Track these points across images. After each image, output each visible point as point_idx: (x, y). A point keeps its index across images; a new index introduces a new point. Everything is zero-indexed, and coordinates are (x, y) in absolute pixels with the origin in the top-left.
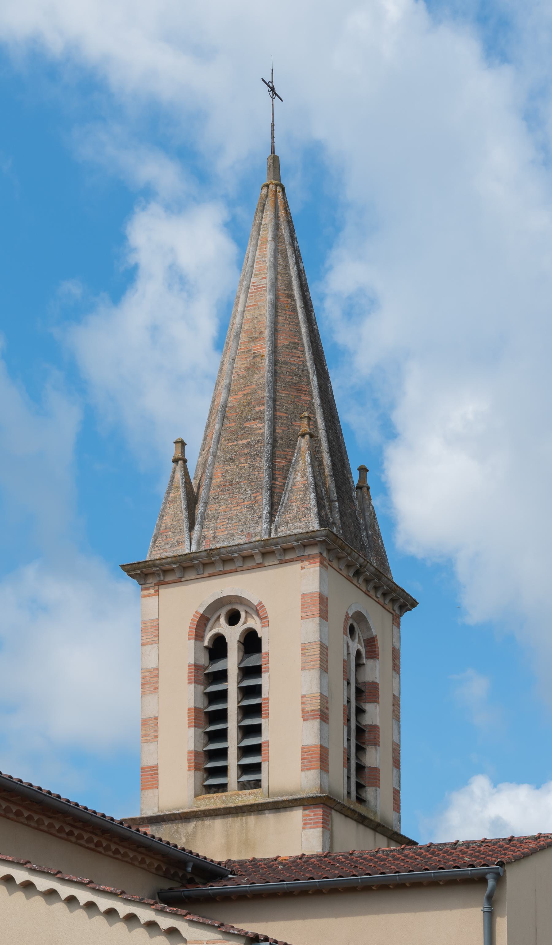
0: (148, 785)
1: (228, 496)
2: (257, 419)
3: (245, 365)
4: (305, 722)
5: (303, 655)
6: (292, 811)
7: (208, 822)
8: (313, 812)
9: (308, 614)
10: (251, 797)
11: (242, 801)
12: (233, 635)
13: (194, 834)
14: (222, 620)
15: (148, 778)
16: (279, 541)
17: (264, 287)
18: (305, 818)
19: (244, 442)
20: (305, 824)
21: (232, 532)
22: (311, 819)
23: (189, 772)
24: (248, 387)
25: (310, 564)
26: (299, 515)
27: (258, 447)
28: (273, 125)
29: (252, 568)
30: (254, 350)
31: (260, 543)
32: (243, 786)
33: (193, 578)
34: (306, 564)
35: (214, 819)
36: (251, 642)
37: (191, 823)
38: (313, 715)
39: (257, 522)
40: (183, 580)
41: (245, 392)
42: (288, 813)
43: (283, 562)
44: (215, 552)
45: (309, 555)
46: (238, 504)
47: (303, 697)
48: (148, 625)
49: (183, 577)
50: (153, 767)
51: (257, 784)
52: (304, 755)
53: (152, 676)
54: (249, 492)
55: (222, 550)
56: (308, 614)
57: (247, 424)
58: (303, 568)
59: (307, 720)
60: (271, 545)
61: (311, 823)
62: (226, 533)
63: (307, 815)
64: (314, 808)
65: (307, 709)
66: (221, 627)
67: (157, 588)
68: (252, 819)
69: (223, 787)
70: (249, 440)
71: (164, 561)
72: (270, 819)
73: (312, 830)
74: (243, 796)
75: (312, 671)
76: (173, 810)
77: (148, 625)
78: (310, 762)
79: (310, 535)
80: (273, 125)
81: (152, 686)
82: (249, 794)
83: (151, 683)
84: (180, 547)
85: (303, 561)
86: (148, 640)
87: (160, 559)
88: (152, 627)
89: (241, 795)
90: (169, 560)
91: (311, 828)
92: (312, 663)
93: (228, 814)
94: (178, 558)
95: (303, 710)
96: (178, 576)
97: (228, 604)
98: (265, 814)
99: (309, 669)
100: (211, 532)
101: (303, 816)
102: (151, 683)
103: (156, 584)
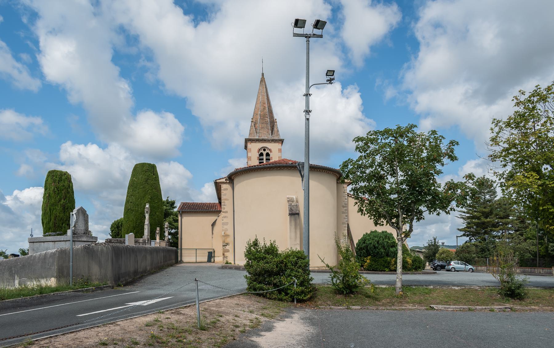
12: (265, 153)
36: (268, 155)
66: (262, 151)
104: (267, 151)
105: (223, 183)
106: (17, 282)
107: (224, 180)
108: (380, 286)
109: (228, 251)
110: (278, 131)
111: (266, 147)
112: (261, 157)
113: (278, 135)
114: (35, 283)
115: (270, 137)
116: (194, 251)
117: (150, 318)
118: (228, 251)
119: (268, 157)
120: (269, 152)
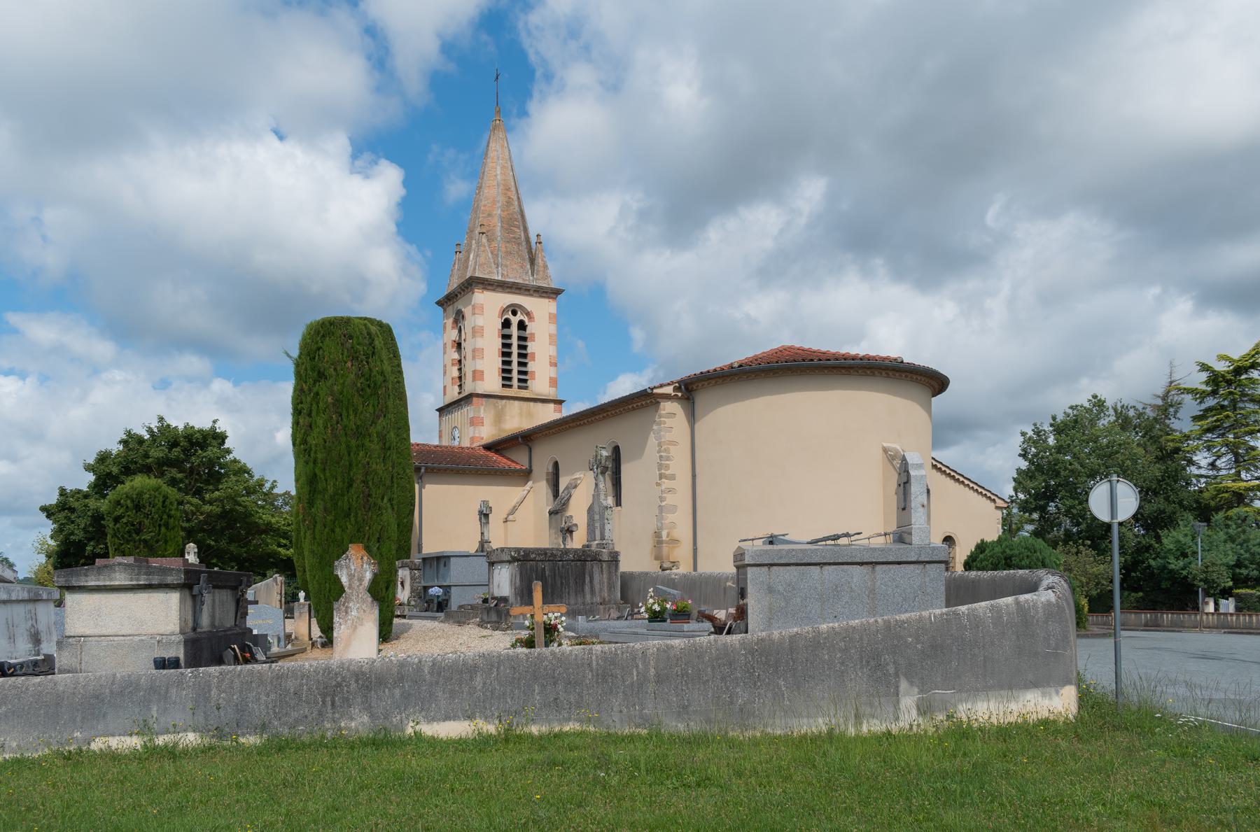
12: (515, 321)
32: (519, 387)
36: (522, 326)
51: (526, 388)
66: (510, 316)
68: (532, 404)
69: (510, 386)
72: (540, 405)
104: (520, 316)
105: (667, 397)
106: (908, 702)
107: (669, 390)
109: (673, 509)
110: (545, 267)
111: (520, 306)
112: (506, 331)
113: (546, 277)
114: (821, 721)
116: (484, 580)
118: (673, 509)
119: (522, 333)
120: (526, 319)
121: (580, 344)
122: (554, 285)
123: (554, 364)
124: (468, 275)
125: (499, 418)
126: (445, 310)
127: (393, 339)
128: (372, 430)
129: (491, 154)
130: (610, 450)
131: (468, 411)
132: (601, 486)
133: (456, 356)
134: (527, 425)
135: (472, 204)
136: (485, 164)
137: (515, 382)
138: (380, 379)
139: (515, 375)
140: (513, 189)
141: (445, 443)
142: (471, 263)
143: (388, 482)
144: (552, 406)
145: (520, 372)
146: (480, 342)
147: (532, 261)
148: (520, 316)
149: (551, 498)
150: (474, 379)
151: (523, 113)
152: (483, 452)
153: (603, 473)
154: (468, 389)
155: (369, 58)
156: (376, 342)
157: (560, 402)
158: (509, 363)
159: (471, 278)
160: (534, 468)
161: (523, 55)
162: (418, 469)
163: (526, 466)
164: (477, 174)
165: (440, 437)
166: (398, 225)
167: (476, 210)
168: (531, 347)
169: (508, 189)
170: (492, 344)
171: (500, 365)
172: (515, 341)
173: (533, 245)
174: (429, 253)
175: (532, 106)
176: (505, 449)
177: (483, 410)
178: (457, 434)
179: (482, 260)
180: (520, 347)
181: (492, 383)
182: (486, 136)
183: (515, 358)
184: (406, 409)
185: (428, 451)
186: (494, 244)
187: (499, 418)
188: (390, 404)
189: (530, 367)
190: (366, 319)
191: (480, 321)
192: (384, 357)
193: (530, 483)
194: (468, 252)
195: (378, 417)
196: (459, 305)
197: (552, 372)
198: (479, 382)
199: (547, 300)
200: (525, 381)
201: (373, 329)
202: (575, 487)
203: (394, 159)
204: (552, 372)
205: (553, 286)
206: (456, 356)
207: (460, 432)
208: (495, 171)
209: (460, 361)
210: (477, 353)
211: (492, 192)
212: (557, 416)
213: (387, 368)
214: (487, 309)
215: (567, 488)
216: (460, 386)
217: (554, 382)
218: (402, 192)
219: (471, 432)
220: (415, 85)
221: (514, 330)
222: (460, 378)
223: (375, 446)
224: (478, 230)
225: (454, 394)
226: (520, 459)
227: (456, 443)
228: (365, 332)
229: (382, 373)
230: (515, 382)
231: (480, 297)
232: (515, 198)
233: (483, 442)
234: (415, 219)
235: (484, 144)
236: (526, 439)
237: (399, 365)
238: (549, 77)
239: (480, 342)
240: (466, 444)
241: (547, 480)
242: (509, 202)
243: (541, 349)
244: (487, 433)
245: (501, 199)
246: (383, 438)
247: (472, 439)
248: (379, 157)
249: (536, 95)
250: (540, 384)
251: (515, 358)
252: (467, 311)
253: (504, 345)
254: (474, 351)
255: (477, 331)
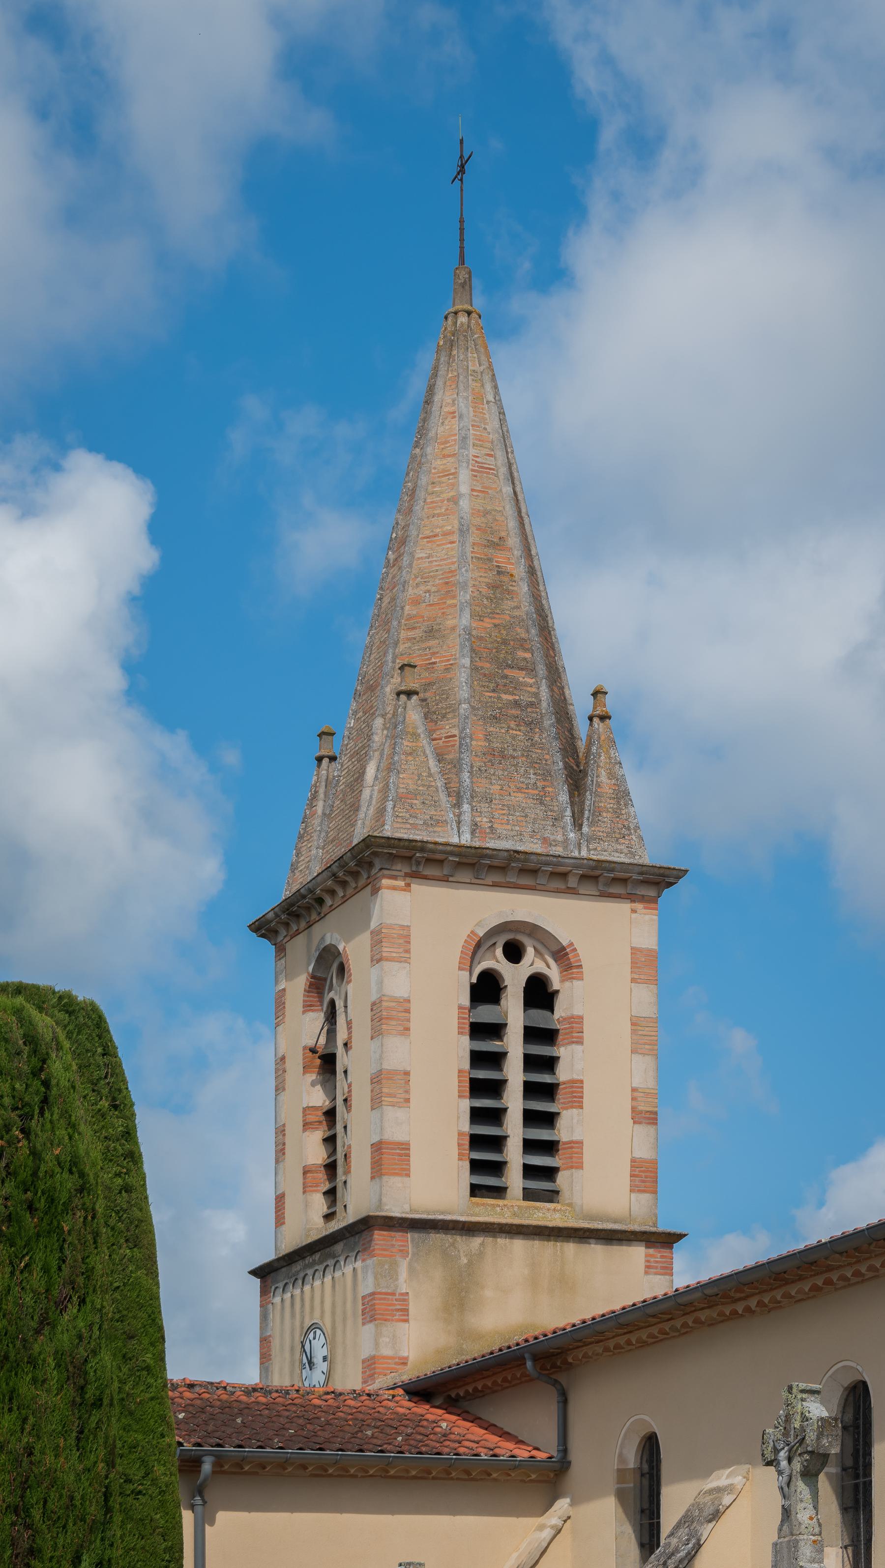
0: (395, 1169)
1: (501, 773)
2: (522, 669)
3: (486, 580)
4: (636, 1126)
5: (634, 1032)
6: (630, 1246)
7: (502, 1241)
8: (660, 1252)
9: (642, 977)
10: (558, 1215)
11: (543, 1218)
12: (514, 978)
13: (481, 1254)
14: (499, 952)
15: (395, 1159)
16: (618, 867)
17: (493, 469)
18: (649, 1258)
19: (511, 698)
20: (647, 1267)
21: (517, 828)
22: (657, 1262)
23: (460, 1163)
24: (497, 616)
25: (645, 908)
26: (614, 832)
27: (533, 712)
28: (462, 221)
29: (557, 892)
30: (496, 562)
31: (591, 862)
32: (529, 1195)
33: (469, 881)
34: (639, 906)
35: (511, 1238)
36: (539, 993)
37: (475, 1238)
38: (649, 1118)
39: (554, 825)
40: (451, 879)
41: (497, 622)
42: (624, 1248)
43: (604, 895)
44: (522, 857)
45: (643, 896)
46: (519, 790)
47: (634, 1090)
48: (394, 931)
49: (452, 876)
50: (403, 1144)
51: (552, 1196)
52: (634, 1171)
53: (401, 1009)
54: (532, 776)
55: (533, 857)
56: (642, 977)
57: (507, 672)
58: (634, 911)
59: (640, 1123)
60: (604, 869)
61: (656, 1268)
62: (509, 827)
63: (651, 1256)
64: (662, 1247)
65: (640, 1108)
66: (497, 961)
67: (408, 880)
68: (570, 1248)
69: (499, 1192)
70: (517, 698)
71: (441, 847)
72: (597, 1251)
73: (659, 1277)
74: (544, 1211)
75: (647, 1057)
76: (423, 1213)
77: (394, 931)
78: (643, 1181)
79: (662, 871)
80: (462, 221)
81: (400, 1025)
82: (554, 1209)
83: (399, 1019)
84: (439, 829)
85: (633, 901)
86: (395, 955)
87: (436, 843)
88: (401, 936)
89: (541, 1209)
90: (449, 848)
91: (656, 1274)
92: (647, 1046)
93: (535, 1234)
94: (464, 850)
95: (634, 1109)
96: (445, 872)
97: (511, 931)
98: (590, 1244)
99: (644, 1054)
100: (485, 820)
101: (646, 1256)
102: (399, 1019)
103: (407, 875)
104: (533, 962)
108: (232, 1449)
110: (622, 796)
111: (533, 930)
112: (486, 1014)
113: (625, 830)
115: (562, 841)
117: (390, 805)
120: (553, 973)
121: (740, 1040)
122: (651, 854)
123: (645, 1117)
124: (360, 833)
125: (459, 1296)
126: (281, 950)
127: (109, 1051)
128: (42, 1346)
129: (441, 427)
130: (836, 1396)
131: (356, 1276)
132: (804, 1515)
133: (318, 1098)
134: (553, 1316)
135: (378, 589)
136: (416, 463)
137: (514, 1179)
138: (67, 1182)
139: (514, 1155)
140: (514, 541)
141: (280, 1379)
142: (369, 793)
143: (94, 1510)
144: (638, 1253)
145: (530, 1146)
146: (397, 1052)
147: (577, 779)
148: (533, 962)
149: (633, 1550)
150: (378, 1170)
151: (553, 275)
152: (404, 1405)
153: (809, 1475)
154: (358, 1202)
155: (41, 111)
156: (56, 1066)
157: (667, 1240)
158: (496, 1116)
159: (368, 842)
160: (576, 1456)
161: (556, 70)
162: (190, 1465)
163: (548, 1450)
164: (395, 491)
165: (265, 1357)
166: (129, 667)
167: (383, 620)
168: (571, 1062)
169: (499, 544)
170: (431, 1056)
171: (466, 1126)
172: (514, 1045)
173: (582, 728)
174: (231, 757)
175: (586, 250)
176: (479, 1395)
177: (411, 1274)
178: (319, 1350)
179: (405, 781)
180: (531, 1062)
181: (437, 1181)
182: (426, 360)
183: (514, 1101)
184: (153, 1273)
185: (226, 1407)
186: (449, 728)
187: (459, 1296)
188: (100, 1261)
189: (568, 1128)
190: (19, 989)
191: (397, 981)
192: (80, 1111)
193: (562, 1505)
194: (361, 758)
195: (61, 1305)
196: (328, 932)
197: (641, 1143)
198: (393, 1183)
199: (625, 907)
200: (550, 1173)
201: (45, 1024)
202: (716, 1516)
203: (114, 447)
204: (641, 1143)
205: (646, 859)
206: (318, 1098)
207: (331, 1343)
208: (454, 486)
209: (330, 1114)
210: (388, 1086)
211: (440, 553)
212: (655, 1287)
213: (89, 1146)
214: (420, 946)
215: (687, 1520)
216: (331, 1194)
217: (644, 1176)
218: (143, 557)
219: (365, 1340)
220: (192, 193)
221: (513, 1011)
222: (331, 1168)
223: (52, 1398)
224: (395, 682)
225: (309, 1219)
226: (532, 1427)
227: (317, 1378)
228: (17, 1034)
229: (74, 1165)
230: (514, 1179)
231: (396, 901)
232: (519, 570)
233: (407, 1375)
234: (179, 647)
235: (417, 386)
236: (549, 1363)
237: (129, 1134)
238: (644, 145)
239: (397, 1052)
240: (349, 1379)
241: (621, 1495)
242: (500, 586)
243: (603, 1066)
244: (420, 1343)
245: (473, 578)
246: (76, 1372)
247: (370, 1365)
248: (64, 448)
249: (599, 207)
250: (597, 1185)
251: (514, 1101)
252: (355, 951)
253: (478, 1059)
254: (377, 1079)
255: (388, 1017)
